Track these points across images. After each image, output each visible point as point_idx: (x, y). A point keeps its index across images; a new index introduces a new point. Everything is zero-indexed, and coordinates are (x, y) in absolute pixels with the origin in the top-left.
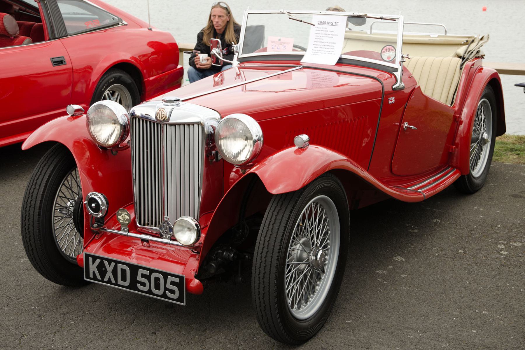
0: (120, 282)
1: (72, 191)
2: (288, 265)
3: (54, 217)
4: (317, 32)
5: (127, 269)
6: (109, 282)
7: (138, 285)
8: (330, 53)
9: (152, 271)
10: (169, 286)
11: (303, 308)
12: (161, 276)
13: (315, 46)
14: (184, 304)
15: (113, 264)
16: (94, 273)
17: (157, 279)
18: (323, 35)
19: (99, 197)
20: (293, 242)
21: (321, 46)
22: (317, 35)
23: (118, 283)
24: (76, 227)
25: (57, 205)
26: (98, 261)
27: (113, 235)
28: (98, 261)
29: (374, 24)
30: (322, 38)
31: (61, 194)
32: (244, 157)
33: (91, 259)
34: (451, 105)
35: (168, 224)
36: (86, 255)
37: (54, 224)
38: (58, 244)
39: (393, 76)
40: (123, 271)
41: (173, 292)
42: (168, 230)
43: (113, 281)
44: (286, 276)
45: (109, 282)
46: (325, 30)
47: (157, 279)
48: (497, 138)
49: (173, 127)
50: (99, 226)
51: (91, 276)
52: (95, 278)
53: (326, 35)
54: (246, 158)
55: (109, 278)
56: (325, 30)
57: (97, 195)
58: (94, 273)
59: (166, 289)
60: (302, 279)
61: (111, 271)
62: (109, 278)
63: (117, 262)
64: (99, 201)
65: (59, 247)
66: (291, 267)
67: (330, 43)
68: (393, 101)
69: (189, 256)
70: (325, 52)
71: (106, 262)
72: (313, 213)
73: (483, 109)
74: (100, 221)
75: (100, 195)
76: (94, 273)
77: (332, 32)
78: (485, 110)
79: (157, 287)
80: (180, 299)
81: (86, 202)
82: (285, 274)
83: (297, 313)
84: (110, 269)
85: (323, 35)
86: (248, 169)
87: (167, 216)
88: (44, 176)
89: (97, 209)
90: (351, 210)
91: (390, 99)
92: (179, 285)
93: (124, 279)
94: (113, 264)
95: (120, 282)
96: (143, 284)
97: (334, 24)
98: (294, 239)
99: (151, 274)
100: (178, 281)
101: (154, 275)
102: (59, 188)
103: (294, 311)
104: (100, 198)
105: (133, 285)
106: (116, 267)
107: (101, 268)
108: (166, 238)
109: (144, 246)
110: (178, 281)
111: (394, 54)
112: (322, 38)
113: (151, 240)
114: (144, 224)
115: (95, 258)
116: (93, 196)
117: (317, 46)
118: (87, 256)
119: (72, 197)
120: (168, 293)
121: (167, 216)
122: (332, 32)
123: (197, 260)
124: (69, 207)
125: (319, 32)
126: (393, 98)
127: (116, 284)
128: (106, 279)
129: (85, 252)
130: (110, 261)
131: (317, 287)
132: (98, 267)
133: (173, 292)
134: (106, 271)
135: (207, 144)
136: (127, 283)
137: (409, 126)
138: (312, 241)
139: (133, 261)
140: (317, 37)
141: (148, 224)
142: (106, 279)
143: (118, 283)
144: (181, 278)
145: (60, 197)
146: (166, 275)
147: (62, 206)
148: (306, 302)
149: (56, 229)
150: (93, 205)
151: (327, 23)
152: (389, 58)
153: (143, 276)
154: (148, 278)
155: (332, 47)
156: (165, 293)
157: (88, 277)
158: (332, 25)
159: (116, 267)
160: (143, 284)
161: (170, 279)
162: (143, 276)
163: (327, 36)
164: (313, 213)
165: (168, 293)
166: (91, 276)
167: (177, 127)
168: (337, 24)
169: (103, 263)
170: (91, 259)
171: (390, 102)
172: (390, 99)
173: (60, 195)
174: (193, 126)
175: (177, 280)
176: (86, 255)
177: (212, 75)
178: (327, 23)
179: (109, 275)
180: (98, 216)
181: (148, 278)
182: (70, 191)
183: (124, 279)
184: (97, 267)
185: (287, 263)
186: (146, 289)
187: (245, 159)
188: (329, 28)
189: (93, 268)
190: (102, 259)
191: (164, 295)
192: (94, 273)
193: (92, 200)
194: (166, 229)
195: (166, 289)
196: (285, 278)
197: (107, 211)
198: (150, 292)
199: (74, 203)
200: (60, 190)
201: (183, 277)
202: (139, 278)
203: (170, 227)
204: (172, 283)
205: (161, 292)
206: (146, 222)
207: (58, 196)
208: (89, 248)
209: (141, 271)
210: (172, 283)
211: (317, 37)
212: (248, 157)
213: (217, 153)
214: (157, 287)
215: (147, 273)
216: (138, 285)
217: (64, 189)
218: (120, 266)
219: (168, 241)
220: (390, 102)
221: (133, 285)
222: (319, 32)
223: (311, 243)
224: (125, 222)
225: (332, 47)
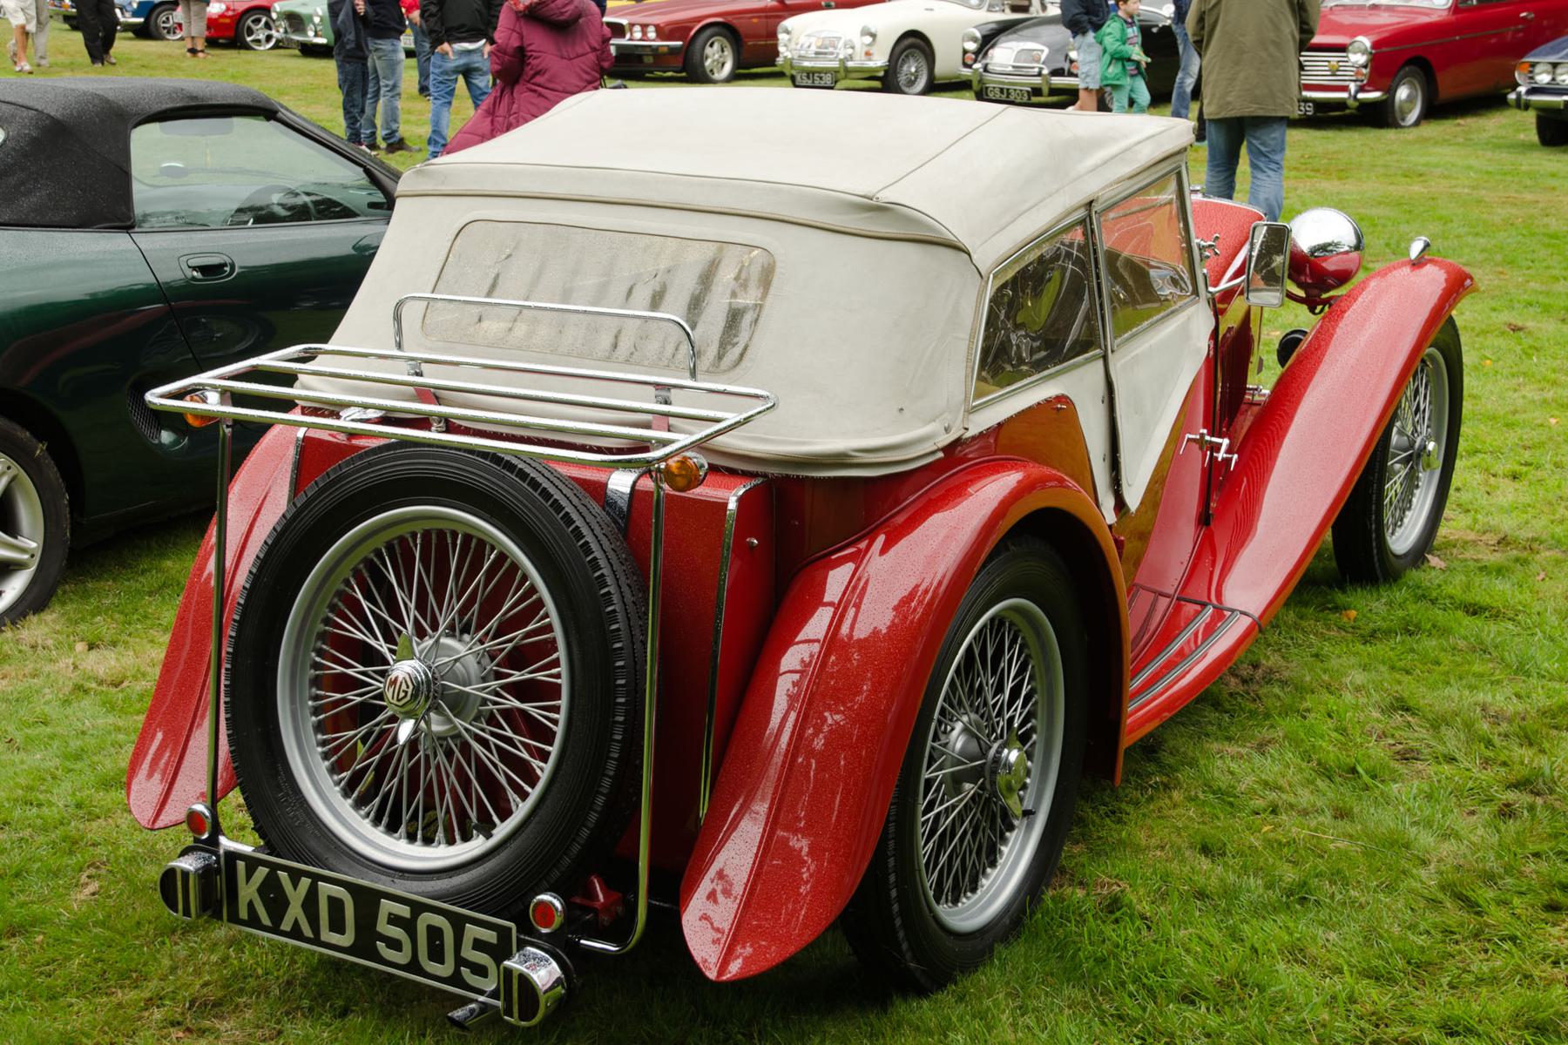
2: (929, 783)
6: (296, 933)
7: (380, 945)
9: (418, 908)
11: (963, 903)
17: (434, 933)
20: (940, 723)
26: (262, 872)
28: (262, 872)
29: (967, 256)
33: (241, 865)
44: (923, 819)
55: (296, 922)
58: (251, 905)
59: (460, 961)
61: (300, 902)
62: (296, 922)
63: (316, 878)
66: (935, 791)
79: (437, 955)
82: (920, 814)
83: (948, 914)
86: (1300, 285)
88: (570, 501)
94: (305, 882)
95: (328, 936)
96: (395, 944)
98: (945, 717)
100: (494, 941)
101: (426, 919)
103: (944, 911)
105: (366, 942)
106: (312, 894)
110: (494, 941)
127: (317, 941)
128: (286, 925)
131: (984, 881)
132: (260, 891)
136: (346, 940)
142: (286, 925)
148: (974, 890)
153: (394, 920)
154: (409, 925)
156: (457, 972)
159: (312, 894)
160: (395, 944)
162: (394, 920)
169: (278, 879)
177: (1323, 267)
179: (295, 912)
181: (409, 925)
183: (337, 926)
185: (926, 775)
190: (274, 868)
192: (251, 905)
195: (460, 961)
196: (920, 824)
198: (414, 966)
202: (384, 927)
204: (479, 945)
205: (445, 970)
209: (387, 906)
210: (479, 945)
215: (404, 911)
216: (380, 945)
221: (366, 942)
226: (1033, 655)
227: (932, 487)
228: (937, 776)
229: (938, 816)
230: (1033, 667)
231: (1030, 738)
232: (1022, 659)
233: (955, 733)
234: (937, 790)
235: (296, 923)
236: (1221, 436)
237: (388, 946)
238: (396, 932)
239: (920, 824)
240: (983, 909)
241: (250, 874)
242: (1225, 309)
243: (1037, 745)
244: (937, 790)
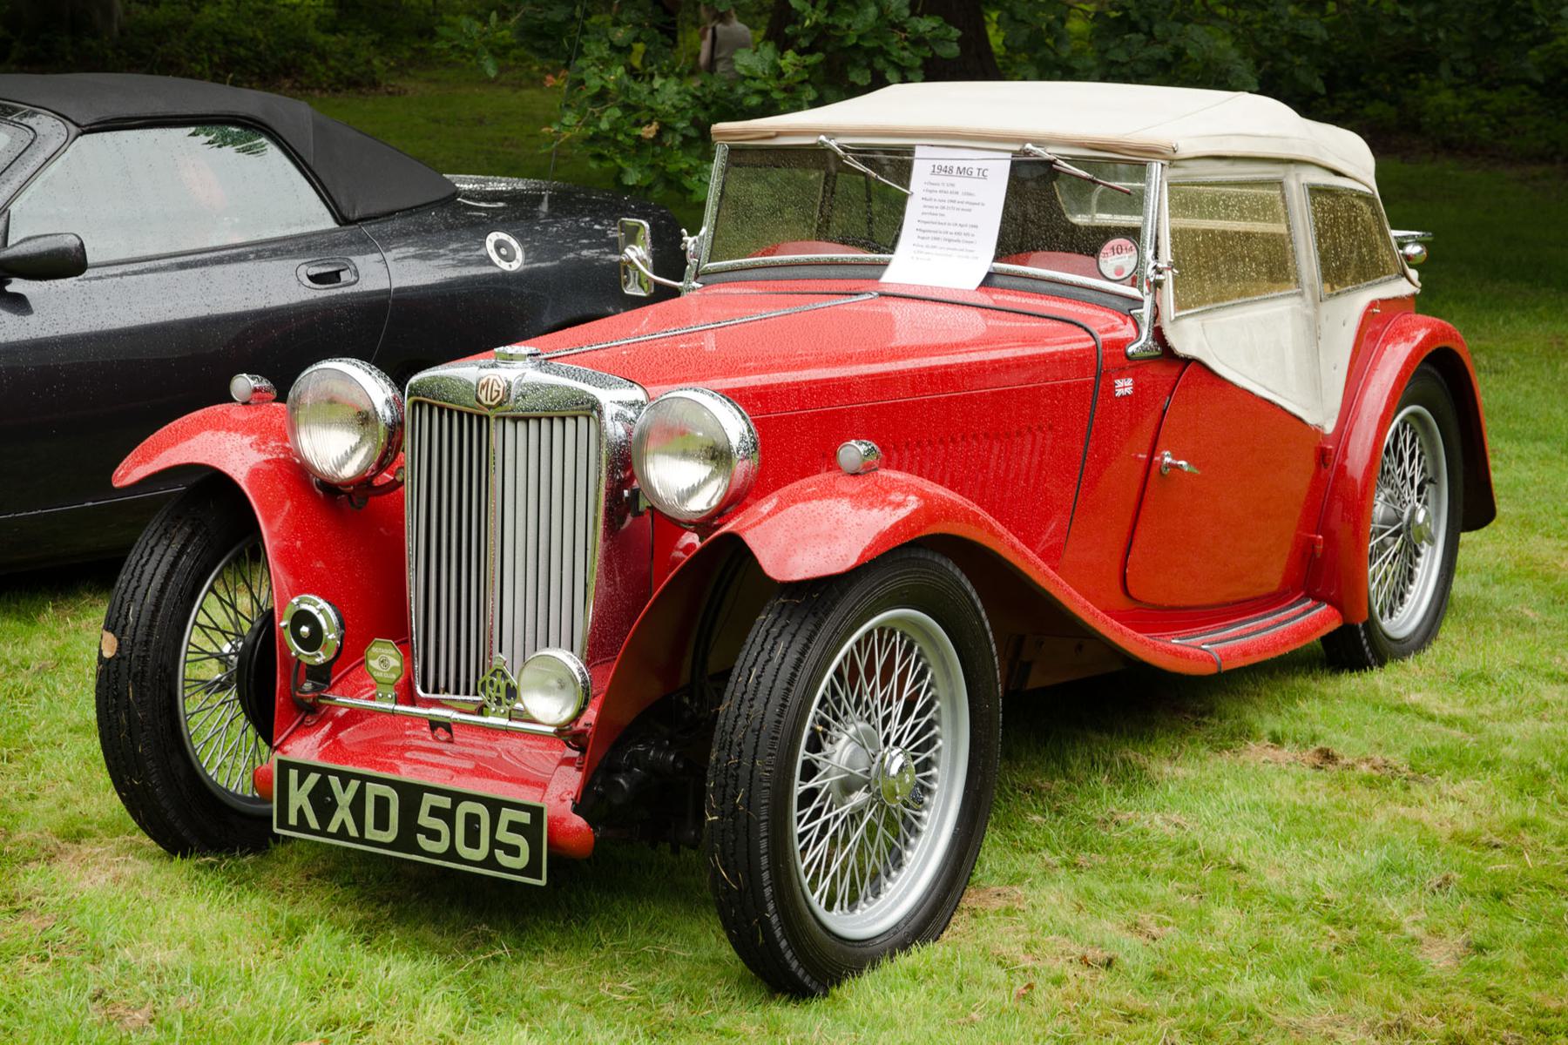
0: (371, 833)
1: (236, 612)
3: (184, 680)
4: (928, 195)
5: (393, 795)
7: (421, 838)
8: (964, 253)
9: (458, 797)
10: (503, 835)
12: (481, 810)
13: (922, 234)
14: (543, 882)
15: (354, 784)
16: (301, 812)
17: (472, 820)
18: (946, 204)
19: (319, 607)
21: (938, 235)
22: (928, 203)
23: (368, 836)
24: (245, 711)
25: (191, 649)
26: (313, 778)
27: (355, 716)
28: (313, 778)
30: (942, 212)
31: (203, 619)
32: (702, 503)
33: (293, 774)
34: (714, 29)
35: (504, 676)
36: (280, 762)
37: (184, 698)
38: (197, 757)
39: (1129, 320)
40: (382, 804)
41: (513, 851)
42: (502, 694)
43: (353, 832)
45: (342, 833)
46: (950, 189)
47: (472, 820)
48: (1465, 537)
49: (521, 426)
50: (315, 688)
51: (293, 820)
52: (303, 825)
53: (951, 205)
54: (709, 503)
55: (343, 823)
56: (950, 189)
57: (315, 604)
58: (301, 811)
59: (495, 844)
60: (862, 839)
62: (343, 823)
63: (364, 779)
64: (321, 618)
65: (201, 765)
67: (961, 226)
68: (1129, 391)
69: (556, 763)
70: (950, 252)
71: (334, 781)
72: (897, 672)
73: (1420, 445)
74: (321, 674)
75: (323, 604)
76: (301, 812)
77: (970, 194)
78: (1426, 451)
79: (472, 840)
80: (532, 869)
81: (283, 624)
84: (345, 798)
85: (946, 204)
87: (501, 651)
89: (314, 641)
90: (1006, 690)
91: (1119, 383)
92: (530, 831)
93: (382, 823)
94: (354, 784)
96: (434, 835)
97: (975, 173)
99: (455, 805)
101: (465, 807)
102: (209, 582)
104: (321, 611)
105: (407, 839)
107: (323, 802)
108: (495, 714)
109: (436, 739)
111: (1134, 261)
112: (942, 212)
113: (456, 722)
114: (436, 691)
115: (304, 770)
116: (304, 606)
117: (925, 235)
118: (284, 767)
119: (235, 627)
120: (499, 854)
121: (501, 651)
122: (970, 194)
123: (579, 769)
124: (227, 655)
125: (933, 196)
126: (1129, 382)
127: (361, 840)
128: (333, 827)
129: (278, 756)
130: (345, 778)
133: (513, 851)
134: (333, 806)
135: (612, 472)
136: (389, 836)
137: (1174, 462)
138: (884, 729)
139: (407, 774)
140: (926, 210)
141: (447, 690)
142: (333, 827)
143: (368, 836)
144: (536, 812)
145: (201, 627)
146: (495, 806)
147: (204, 652)
149: (193, 714)
150: (305, 630)
151: (955, 170)
152: (1119, 271)
153: (435, 812)
155: (968, 238)
156: (491, 855)
157: (283, 823)
158: (970, 175)
160: (434, 835)
161: (507, 815)
162: (435, 812)
163: (956, 205)
164: (897, 672)
165: (499, 854)
166: (293, 820)
167: (533, 424)
168: (982, 174)
170: (293, 774)
171: (1119, 393)
172: (1119, 383)
173: (200, 620)
174: (573, 422)
175: (525, 818)
176: (280, 762)
178: (955, 170)
179: (343, 815)
180: (318, 660)
181: (448, 816)
182: (231, 612)
183: (382, 823)
184: (310, 796)
186: (441, 847)
187: (705, 508)
188: (961, 183)
189: (299, 798)
190: (325, 772)
191: (491, 862)
192: (301, 811)
193: (302, 617)
194: (498, 691)
196: (796, 839)
197: (339, 650)
198: (451, 854)
199: (240, 645)
200: (201, 607)
201: (541, 810)
202: (424, 820)
203: (508, 685)
204: (514, 827)
205: (480, 854)
206: (442, 684)
207: (195, 623)
208: (287, 748)
209: (429, 800)
210: (514, 827)
211: (926, 210)
212: (714, 503)
213: (635, 494)
214: (472, 840)
215: (446, 803)
216: (421, 838)
217: (212, 604)
218: (372, 790)
219: (504, 722)
220: (1119, 393)
221: (407, 839)
222: (933, 196)
223: (882, 738)
224: (386, 676)
225: (968, 238)
226: (932, 663)
227: (839, 361)
228: (824, 785)
229: (827, 822)
230: (932, 676)
231: (935, 743)
232: (919, 668)
233: (842, 743)
234: (824, 799)
235: (343, 825)
236: (1170, 465)
237: (428, 838)
238: (439, 825)
239: (796, 839)
240: (859, 927)
241: (301, 781)
242: (890, 260)
243: (943, 752)
244: (824, 799)
